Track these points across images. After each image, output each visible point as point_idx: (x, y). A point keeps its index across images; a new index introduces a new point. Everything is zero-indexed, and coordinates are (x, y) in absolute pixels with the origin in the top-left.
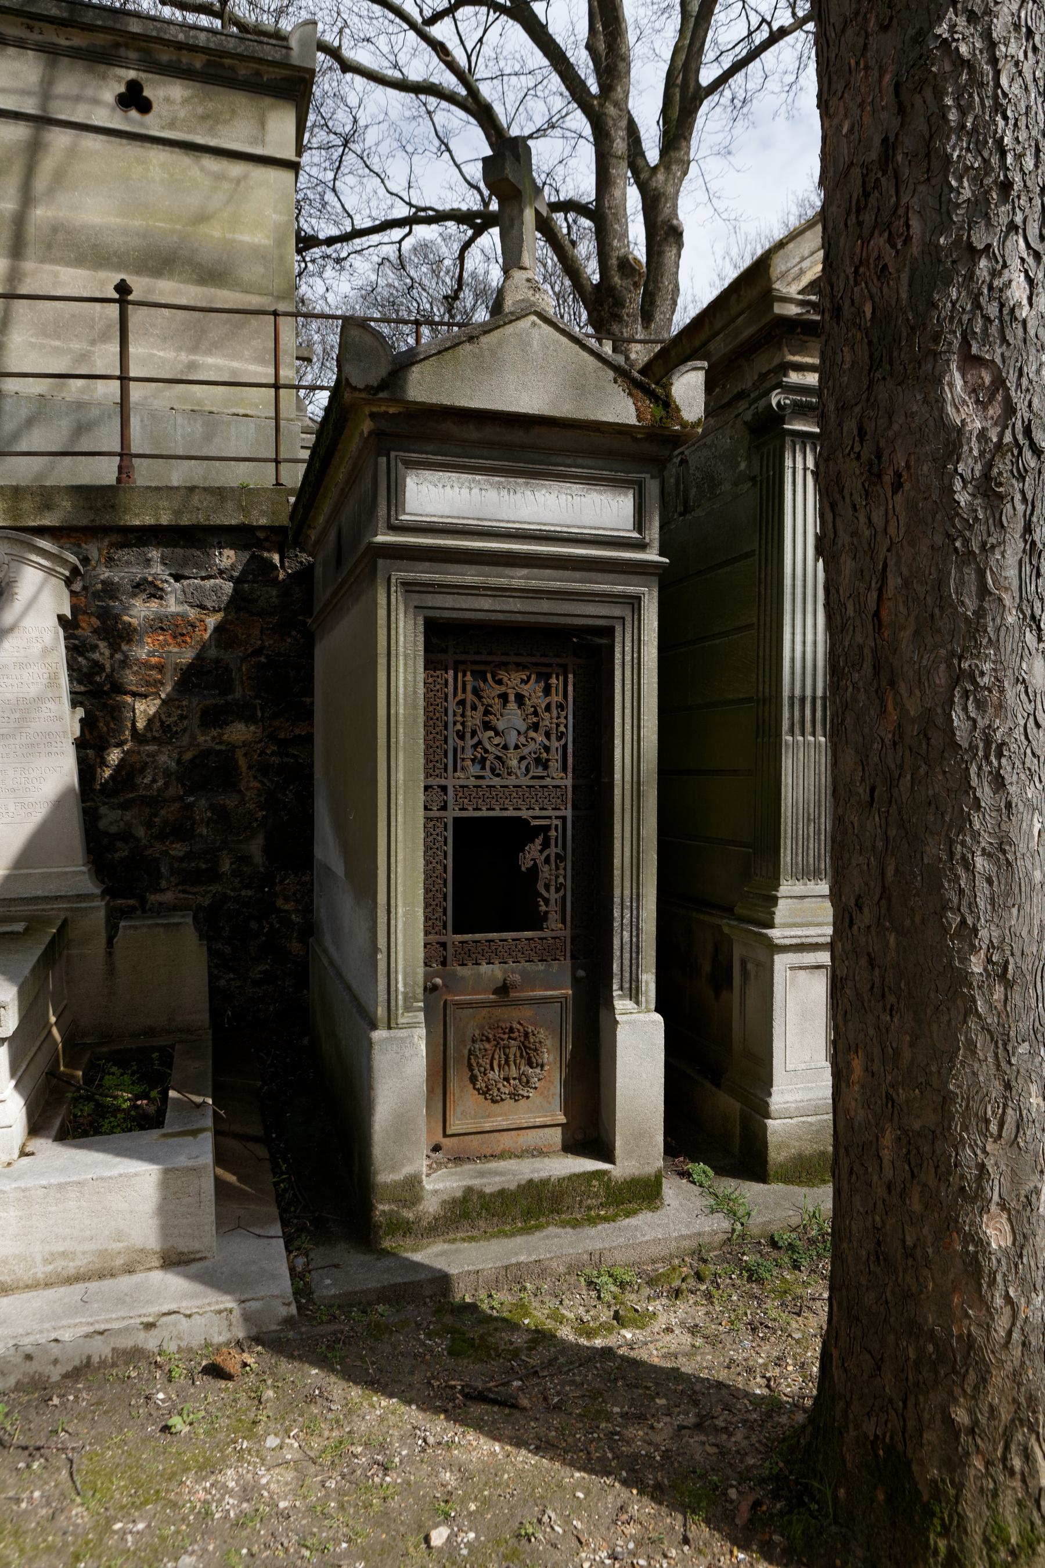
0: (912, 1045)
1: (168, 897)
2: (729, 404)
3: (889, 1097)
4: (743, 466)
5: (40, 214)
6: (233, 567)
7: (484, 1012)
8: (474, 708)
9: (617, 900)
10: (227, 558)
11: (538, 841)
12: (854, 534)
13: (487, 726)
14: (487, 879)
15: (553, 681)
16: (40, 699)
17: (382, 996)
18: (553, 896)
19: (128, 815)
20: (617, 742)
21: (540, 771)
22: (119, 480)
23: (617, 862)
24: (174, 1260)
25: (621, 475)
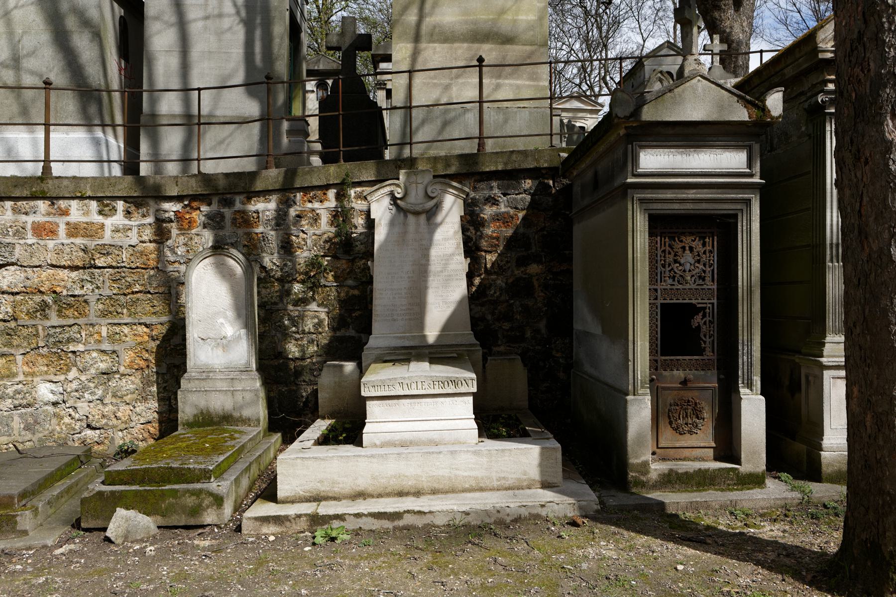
0: (877, 378)
1: (502, 348)
2: (796, 97)
3: (869, 401)
4: (803, 129)
5: (429, 21)
6: (531, 188)
7: (675, 392)
8: (670, 253)
9: (740, 341)
10: (528, 184)
11: (701, 314)
12: (850, 180)
13: (676, 261)
14: (676, 332)
15: (707, 240)
16: (453, 254)
17: (631, 381)
18: (708, 340)
19: (484, 309)
20: (740, 267)
21: (701, 282)
22: (479, 150)
23: (740, 323)
24: (546, 485)
25: (741, 143)
